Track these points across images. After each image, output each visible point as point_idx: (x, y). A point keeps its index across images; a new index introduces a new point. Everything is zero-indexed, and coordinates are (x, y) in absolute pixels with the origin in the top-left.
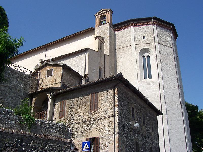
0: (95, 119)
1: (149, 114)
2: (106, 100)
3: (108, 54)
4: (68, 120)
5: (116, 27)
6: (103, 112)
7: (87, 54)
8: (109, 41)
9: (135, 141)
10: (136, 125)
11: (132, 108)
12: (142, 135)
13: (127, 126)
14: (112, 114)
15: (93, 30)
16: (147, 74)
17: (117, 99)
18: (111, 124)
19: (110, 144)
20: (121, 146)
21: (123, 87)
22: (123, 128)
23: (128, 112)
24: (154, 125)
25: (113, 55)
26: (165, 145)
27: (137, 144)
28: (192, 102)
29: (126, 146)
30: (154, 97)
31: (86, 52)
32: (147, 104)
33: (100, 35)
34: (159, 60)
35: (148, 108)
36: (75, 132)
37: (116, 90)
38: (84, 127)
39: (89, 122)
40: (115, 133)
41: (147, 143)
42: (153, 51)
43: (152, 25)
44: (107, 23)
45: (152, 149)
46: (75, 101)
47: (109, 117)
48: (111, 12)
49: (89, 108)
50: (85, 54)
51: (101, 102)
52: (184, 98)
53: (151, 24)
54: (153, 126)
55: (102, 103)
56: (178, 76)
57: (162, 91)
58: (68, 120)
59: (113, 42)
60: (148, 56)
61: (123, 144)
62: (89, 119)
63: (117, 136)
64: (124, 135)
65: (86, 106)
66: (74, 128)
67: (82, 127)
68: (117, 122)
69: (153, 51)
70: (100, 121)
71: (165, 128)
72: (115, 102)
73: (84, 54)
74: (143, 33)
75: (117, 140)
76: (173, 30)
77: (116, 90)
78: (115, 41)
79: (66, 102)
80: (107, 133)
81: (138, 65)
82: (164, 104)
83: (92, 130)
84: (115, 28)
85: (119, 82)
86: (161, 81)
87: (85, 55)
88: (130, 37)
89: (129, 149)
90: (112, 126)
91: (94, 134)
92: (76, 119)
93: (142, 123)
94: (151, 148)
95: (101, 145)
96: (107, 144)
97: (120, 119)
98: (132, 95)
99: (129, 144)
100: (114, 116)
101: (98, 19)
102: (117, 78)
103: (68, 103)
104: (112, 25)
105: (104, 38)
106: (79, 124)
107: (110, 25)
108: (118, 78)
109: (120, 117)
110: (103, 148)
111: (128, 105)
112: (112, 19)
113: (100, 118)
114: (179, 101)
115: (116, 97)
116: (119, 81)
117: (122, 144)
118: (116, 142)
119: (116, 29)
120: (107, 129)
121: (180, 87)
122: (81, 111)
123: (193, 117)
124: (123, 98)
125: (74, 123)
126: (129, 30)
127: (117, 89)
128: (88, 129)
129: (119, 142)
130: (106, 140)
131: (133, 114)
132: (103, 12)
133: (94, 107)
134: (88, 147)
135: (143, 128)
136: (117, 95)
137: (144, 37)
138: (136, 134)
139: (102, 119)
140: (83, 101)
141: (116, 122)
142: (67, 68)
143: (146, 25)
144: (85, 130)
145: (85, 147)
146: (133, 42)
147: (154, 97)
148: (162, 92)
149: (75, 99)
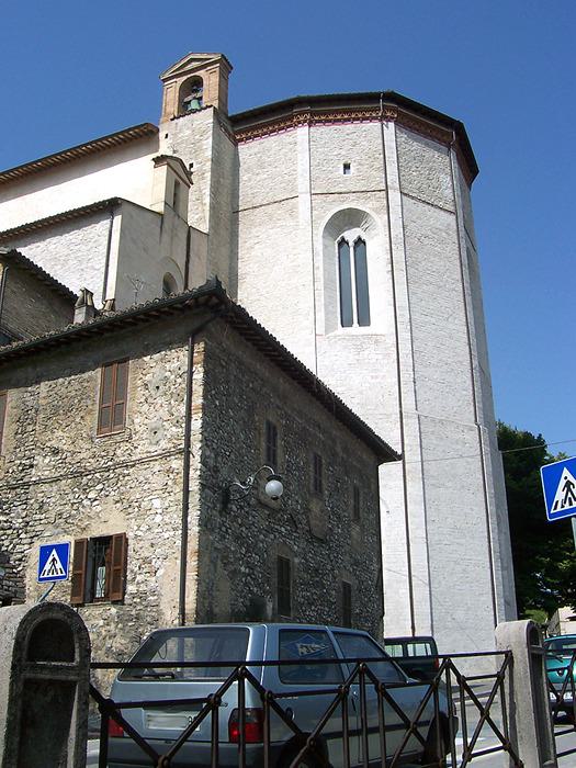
0: (114, 465)
1: (341, 454)
2: (158, 388)
3: (205, 227)
4: (11, 471)
5: (240, 125)
6: (145, 436)
7: (118, 220)
8: (209, 178)
9: (274, 554)
10: (273, 486)
11: (269, 423)
12: (310, 531)
13: (239, 491)
14: (179, 442)
15: (152, 132)
16: (353, 307)
17: (200, 382)
18: (175, 483)
19: (166, 563)
20: (212, 568)
21: (227, 339)
22: (222, 499)
23: (247, 438)
24: (361, 498)
25: (225, 234)
26: (413, 578)
27: (284, 566)
28: (519, 424)
29: (235, 572)
30: (377, 398)
31: (113, 215)
32: (330, 410)
33: (174, 152)
34: (399, 255)
35: (339, 432)
36: (38, 517)
37: (199, 347)
38: (71, 496)
39: (89, 477)
40: (189, 519)
41: (329, 567)
42: (379, 220)
43: (381, 120)
44: (208, 107)
45: (350, 592)
46: (42, 395)
47: (166, 455)
48: (226, 67)
49: (92, 421)
50: (108, 221)
51: (140, 393)
52: (491, 405)
53: (376, 118)
54: (357, 501)
55: (142, 400)
56: (471, 321)
57: (409, 371)
58: (11, 471)
59: (227, 182)
60: (360, 239)
61: (219, 562)
62: (91, 464)
63: (194, 529)
64: (224, 529)
65: (82, 414)
66: (31, 502)
67: (63, 494)
68: (198, 473)
69: (379, 220)
70: (131, 470)
71: (415, 517)
72: (191, 396)
73: (105, 221)
74: (343, 153)
75: (193, 545)
76: (460, 145)
77: (199, 347)
78: (234, 180)
79: (8, 400)
80: (158, 519)
81: (320, 274)
82: (411, 427)
83: (99, 508)
84: (236, 129)
85: (208, 316)
86: (404, 335)
87: (108, 226)
88: (289, 162)
89: (246, 584)
90: (179, 489)
91: (107, 522)
92: (44, 466)
93: (312, 488)
94: (347, 587)
95: (133, 565)
96: (154, 561)
97: (211, 462)
98: (267, 374)
99: (248, 563)
100: (187, 453)
101: (172, 93)
102: (202, 300)
103: (14, 404)
104: (226, 114)
105: (191, 165)
106: (54, 484)
107: (220, 115)
108: (207, 301)
109: (209, 457)
110: (139, 578)
111: (251, 411)
112: (227, 95)
113: (134, 458)
114: (473, 412)
115: (199, 376)
116: (213, 315)
117: (213, 562)
118: (189, 552)
119: (239, 132)
120: (157, 503)
121: (475, 363)
122: (61, 433)
123: (524, 479)
124: (227, 382)
125: (33, 479)
126: (291, 139)
127: (202, 345)
128: (86, 502)
129: (200, 553)
130: (152, 545)
131: (317, 476)
132: (195, 64)
133: (112, 416)
134: (59, 565)
135: (315, 507)
136: (201, 369)
137: (347, 167)
138: (283, 529)
139: (141, 461)
140: (73, 393)
141: (194, 474)
142: (25, 269)
143: (354, 119)
144: (75, 507)
145: (48, 566)
146: (303, 185)
147: (377, 398)
148: (407, 376)
149: (44, 387)
